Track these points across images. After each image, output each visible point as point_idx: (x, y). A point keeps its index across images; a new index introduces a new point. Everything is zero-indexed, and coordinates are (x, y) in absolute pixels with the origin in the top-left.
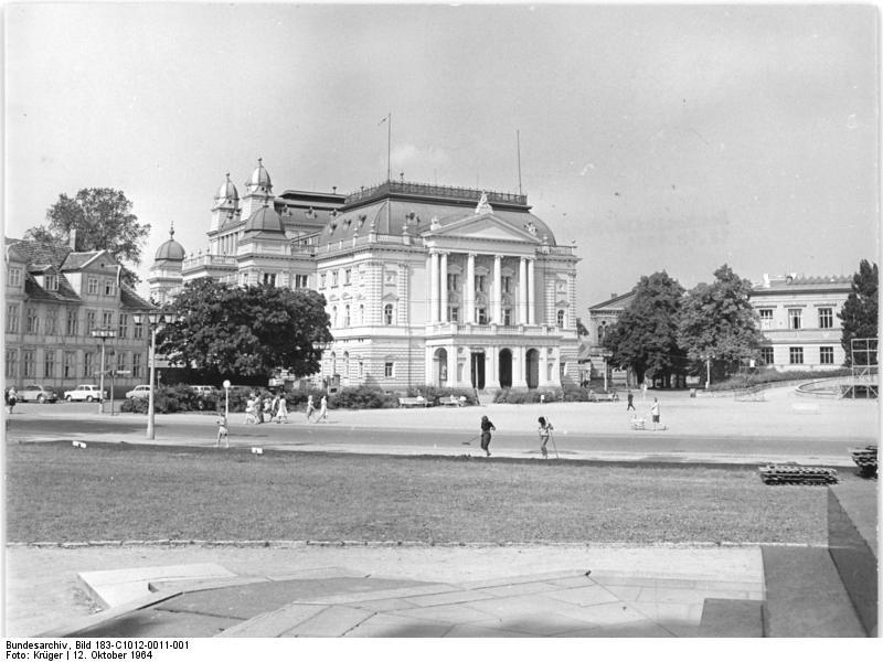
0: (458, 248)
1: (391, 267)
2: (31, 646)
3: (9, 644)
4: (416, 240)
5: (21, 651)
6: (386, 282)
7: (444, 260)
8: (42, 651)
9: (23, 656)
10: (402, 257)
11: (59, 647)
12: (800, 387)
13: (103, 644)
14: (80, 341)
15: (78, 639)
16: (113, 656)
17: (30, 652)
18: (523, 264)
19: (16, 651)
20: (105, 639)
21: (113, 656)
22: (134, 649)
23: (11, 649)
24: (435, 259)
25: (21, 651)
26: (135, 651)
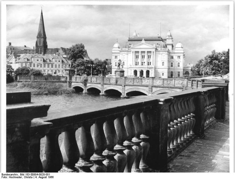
0: (137, 50)
1: (123, 54)
2: (8, 175)
3: (2, 174)
4: (129, 49)
5: (6, 176)
6: (123, 57)
7: (134, 53)
8: (11, 176)
9: (6, 177)
10: (126, 53)
11: (16, 175)
12: (182, 91)
13: (27, 174)
14: (54, 69)
15: (21, 173)
16: (30, 177)
17: (8, 176)
18: (152, 52)
19: (4, 176)
20: (28, 173)
21: (30, 177)
22: (49, 176)
23: (3, 176)
24: (132, 52)
25: (6, 176)
26: (49, 176)
